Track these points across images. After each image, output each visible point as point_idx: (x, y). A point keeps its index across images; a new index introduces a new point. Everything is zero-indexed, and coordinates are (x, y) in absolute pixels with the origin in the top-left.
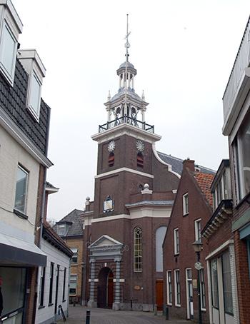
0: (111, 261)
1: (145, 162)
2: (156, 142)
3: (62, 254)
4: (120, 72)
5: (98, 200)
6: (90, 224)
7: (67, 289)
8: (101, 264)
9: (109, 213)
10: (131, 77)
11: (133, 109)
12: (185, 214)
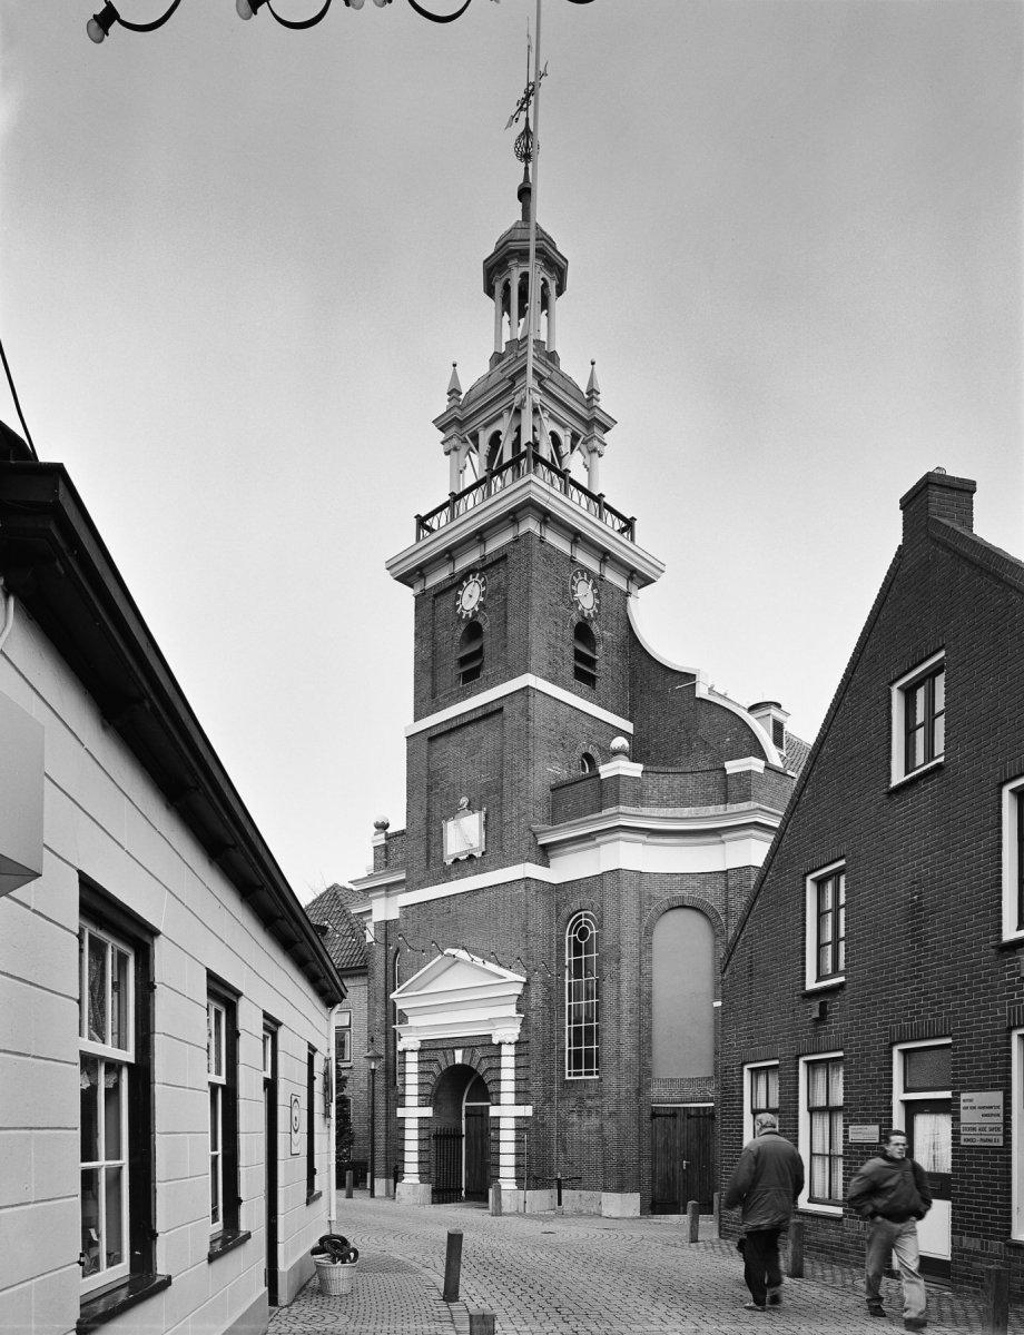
1: (600, 665)
4: (495, 269)
6: (394, 914)
7: (582, 512)
9: (468, 864)
10: (545, 304)
12: (898, 777)
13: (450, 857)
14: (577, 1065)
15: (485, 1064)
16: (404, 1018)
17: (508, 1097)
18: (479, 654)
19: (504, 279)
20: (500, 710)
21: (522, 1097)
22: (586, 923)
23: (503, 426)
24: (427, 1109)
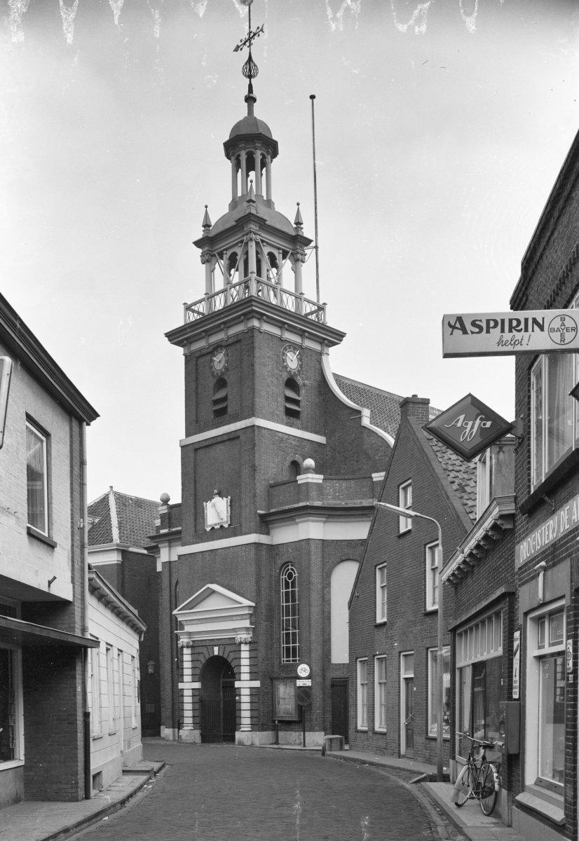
0: (236, 646)
2: (332, 350)
3: (124, 626)
4: (231, 148)
5: (191, 502)
6: (174, 558)
8: (204, 650)
9: (217, 347)
10: (263, 165)
11: (271, 256)
13: (210, 526)
14: (288, 656)
15: (232, 656)
16: (180, 625)
17: (245, 676)
18: (225, 399)
19: (236, 155)
20: (238, 437)
21: (254, 676)
22: (292, 569)
23: (239, 250)
24: (198, 683)
